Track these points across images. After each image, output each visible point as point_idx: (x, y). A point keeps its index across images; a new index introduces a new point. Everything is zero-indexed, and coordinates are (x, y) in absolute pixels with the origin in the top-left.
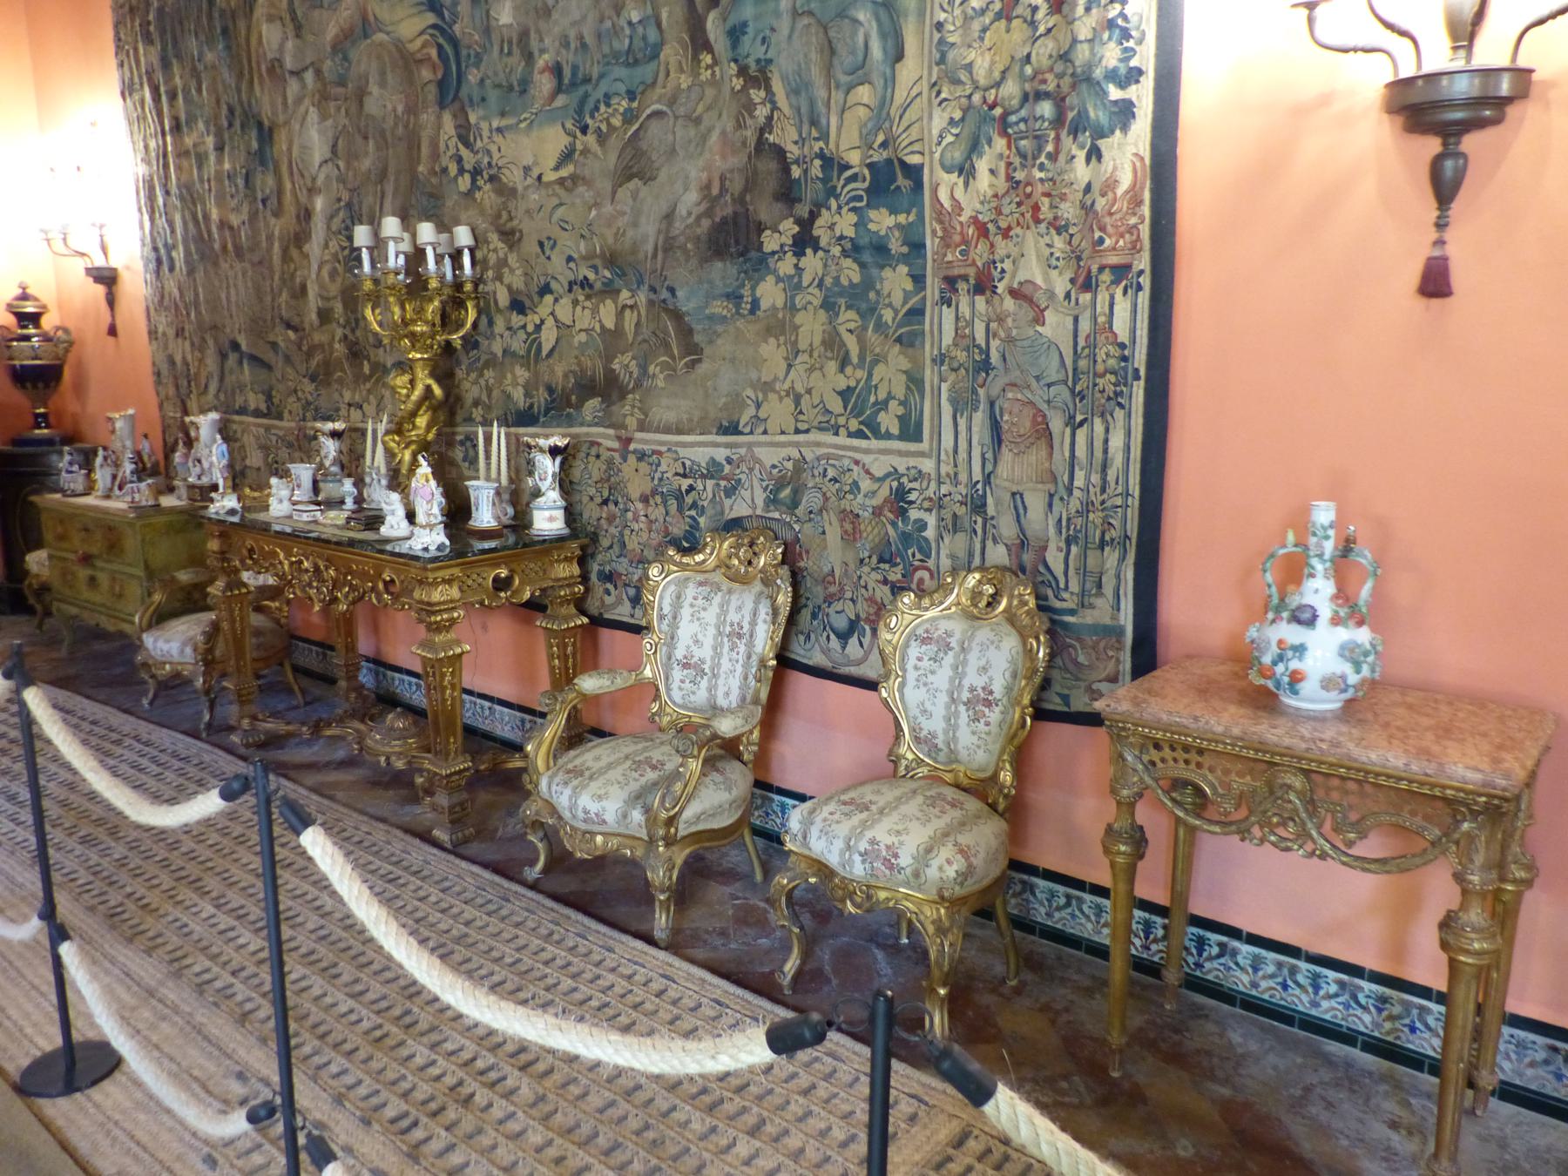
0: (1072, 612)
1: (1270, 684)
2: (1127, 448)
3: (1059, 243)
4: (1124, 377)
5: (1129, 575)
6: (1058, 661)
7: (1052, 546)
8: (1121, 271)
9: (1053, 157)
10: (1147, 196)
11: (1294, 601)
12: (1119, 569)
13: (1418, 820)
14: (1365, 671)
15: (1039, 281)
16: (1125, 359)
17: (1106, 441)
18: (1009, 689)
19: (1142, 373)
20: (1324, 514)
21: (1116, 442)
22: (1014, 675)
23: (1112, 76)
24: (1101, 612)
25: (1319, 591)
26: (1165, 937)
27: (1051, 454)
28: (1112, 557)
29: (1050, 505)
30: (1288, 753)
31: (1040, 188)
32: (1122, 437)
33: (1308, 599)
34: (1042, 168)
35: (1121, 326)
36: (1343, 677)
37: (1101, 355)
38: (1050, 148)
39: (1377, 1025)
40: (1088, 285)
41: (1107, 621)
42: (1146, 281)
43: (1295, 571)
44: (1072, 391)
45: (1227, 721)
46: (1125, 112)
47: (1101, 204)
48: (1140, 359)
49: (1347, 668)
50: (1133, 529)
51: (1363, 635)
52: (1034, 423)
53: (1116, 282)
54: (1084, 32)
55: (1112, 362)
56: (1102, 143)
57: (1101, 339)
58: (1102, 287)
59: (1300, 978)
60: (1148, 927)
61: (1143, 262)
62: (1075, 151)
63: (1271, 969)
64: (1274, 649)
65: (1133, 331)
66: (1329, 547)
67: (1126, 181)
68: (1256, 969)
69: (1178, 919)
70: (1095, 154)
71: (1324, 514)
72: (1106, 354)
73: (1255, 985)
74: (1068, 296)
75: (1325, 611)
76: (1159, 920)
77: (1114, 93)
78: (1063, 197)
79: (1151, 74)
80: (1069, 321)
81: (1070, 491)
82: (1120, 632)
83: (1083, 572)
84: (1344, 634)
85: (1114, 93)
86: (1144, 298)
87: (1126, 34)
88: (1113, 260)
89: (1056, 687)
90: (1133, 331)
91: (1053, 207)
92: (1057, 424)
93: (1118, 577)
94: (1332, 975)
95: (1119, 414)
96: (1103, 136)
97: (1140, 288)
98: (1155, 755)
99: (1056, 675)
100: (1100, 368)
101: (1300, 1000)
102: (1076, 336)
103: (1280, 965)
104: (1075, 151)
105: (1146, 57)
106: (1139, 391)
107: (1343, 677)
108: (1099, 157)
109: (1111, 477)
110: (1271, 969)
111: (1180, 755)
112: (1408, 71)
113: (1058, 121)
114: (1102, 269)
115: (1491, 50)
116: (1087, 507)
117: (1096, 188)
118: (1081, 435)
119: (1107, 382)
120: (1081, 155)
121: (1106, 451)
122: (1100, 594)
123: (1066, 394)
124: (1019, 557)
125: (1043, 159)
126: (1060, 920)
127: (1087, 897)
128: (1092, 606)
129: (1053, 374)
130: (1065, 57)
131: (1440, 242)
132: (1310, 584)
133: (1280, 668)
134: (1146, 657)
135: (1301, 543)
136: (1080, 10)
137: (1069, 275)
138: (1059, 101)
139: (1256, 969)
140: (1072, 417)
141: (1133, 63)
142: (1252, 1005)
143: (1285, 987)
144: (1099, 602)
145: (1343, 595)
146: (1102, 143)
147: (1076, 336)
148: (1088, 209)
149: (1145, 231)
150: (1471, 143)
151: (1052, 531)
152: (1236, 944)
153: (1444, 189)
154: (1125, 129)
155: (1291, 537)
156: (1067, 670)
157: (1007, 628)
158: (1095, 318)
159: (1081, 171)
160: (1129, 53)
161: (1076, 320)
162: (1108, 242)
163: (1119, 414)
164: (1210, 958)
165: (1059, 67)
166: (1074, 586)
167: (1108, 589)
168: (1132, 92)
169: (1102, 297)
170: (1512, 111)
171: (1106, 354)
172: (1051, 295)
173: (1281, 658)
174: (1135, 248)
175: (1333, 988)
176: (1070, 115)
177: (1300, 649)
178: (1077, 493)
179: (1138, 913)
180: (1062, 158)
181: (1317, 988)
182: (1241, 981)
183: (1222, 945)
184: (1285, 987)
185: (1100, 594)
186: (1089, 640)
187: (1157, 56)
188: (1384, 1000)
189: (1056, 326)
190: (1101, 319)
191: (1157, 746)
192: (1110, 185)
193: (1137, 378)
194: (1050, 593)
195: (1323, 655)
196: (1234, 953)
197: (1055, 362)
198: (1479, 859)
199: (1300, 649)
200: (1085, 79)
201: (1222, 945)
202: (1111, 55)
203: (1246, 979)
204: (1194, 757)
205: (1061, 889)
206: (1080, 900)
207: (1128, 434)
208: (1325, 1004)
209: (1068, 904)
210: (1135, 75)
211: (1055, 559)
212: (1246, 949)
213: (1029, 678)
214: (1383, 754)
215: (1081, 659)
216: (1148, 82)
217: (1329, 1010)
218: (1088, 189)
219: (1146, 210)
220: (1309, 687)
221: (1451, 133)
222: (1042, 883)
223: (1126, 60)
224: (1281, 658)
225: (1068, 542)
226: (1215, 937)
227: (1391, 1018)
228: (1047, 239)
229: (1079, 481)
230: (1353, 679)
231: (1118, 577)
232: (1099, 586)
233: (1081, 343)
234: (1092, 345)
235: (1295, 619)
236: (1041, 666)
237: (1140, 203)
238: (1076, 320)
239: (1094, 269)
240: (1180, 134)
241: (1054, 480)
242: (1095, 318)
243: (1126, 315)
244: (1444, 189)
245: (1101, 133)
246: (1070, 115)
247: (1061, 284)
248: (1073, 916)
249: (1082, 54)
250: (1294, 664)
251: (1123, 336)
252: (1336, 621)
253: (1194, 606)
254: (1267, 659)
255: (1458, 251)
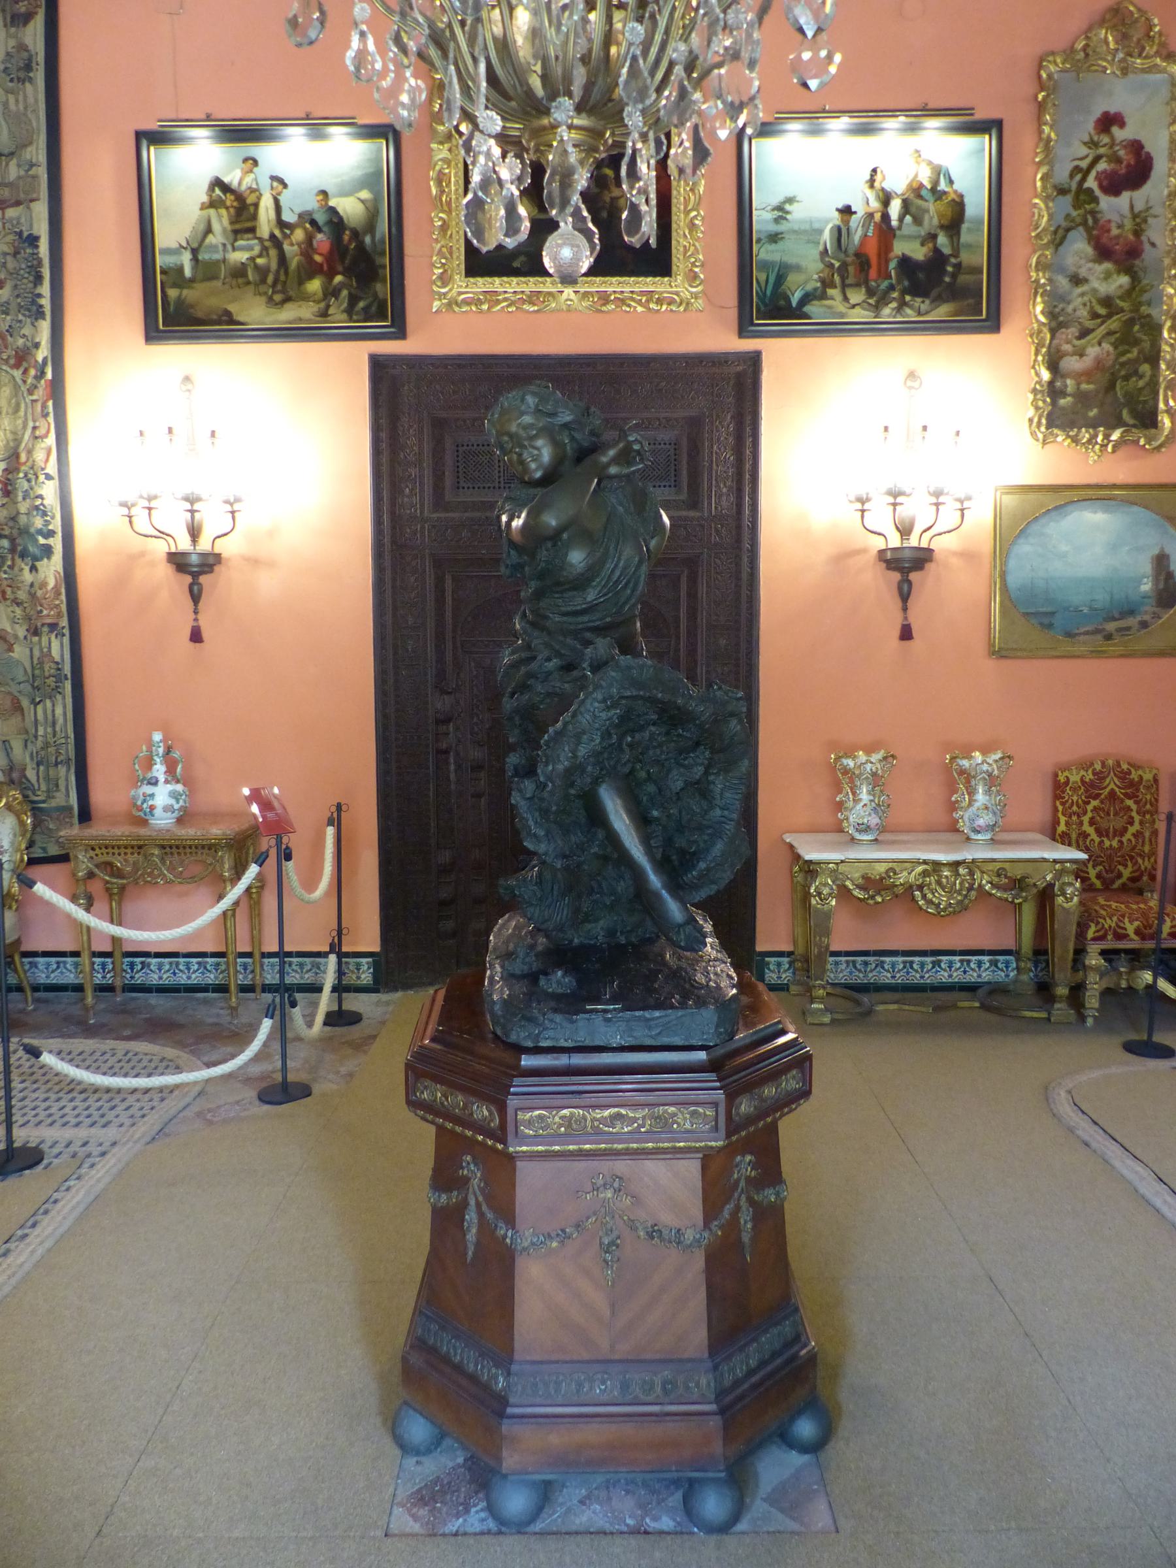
0: (44, 802)
1: (141, 814)
2: (65, 714)
3: (18, 611)
4: (59, 678)
5: (73, 778)
6: (38, 829)
7: (29, 768)
8: (53, 627)
9: (11, 567)
10: (63, 591)
11: (149, 775)
12: (67, 776)
13: (204, 856)
14: (181, 803)
15: (9, 630)
16: (59, 669)
17: (53, 711)
18: (12, 843)
19: (69, 676)
20: (157, 737)
21: (59, 711)
22: (15, 835)
23: (40, 532)
24: (59, 800)
25: (159, 770)
26: (113, 969)
27: (23, 719)
28: (62, 770)
29: (26, 746)
30: (150, 838)
31: (5, 583)
32: (62, 709)
33: (155, 774)
34: (5, 572)
35: (55, 652)
36: (172, 806)
37: (47, 668)
38: (9, 563)
39: (216, 978)
40: (36, 632)
41: (63, 803)
42: (66, 631)
43: (149, 763)
44: (33, 686)
45: (122, 831)
46: (48, 551)
47: (39, 593)
48: (67, 669)
49: (173, 802)
50: (72, 755)
51: (179, 787)
52: (13, 703)
53: (51, 632)
54: (23, 510)
55: (52, 671)
56: (37, 564)
57: (46, 659)
58: (44, 634)
59: (181, 967)
60: (104, 965)
61: (64, 622)
62: (23, 566)
63: (167, 967)
64: (142, 797)
65: (62, 656)
66: (161, 750)
67: (51, 583)
68: (160, 970)
69: (117, 955)
70: (34, 569)
71: (157, 737)
72: (49, 668)
73: (161, 978)
74: (25, 638)
75: (162, 778)
76: (109, 960)
77: (42, 541)
78: (19, 588)
79: (60, 534)
80: (27, 651)
81: (36, 737)
82: (70, 808)
83: (47, 779)
84: (170, 787)
85: (42, 541)
86: (66, 640)
87: (45, 514)
88: (49, 621)
89: (39, 844)
90: (62, 656)
91: (13, 592)
92: (25, 703)
93: (67, 780)
94: (194, 960)
95: (59, 697)
96: (38, 560)
97: (64, 635)
98: (92, 853)
99: (37, 837)
100: (47, 674)
101: (182, 979)
102: (32, 658)
103: (171, 963)
104: (23, 566)
105: (57, 524)
106: (68, 685)
107: (172, 806)
108: (37, 570)
109: (58, 729)
110: (167, 967)
111: (104, 850)
112: (173, 550)
113: (13, 550)
114: (43, 625)
115: (204, 545)
116: (46, 745)
117: (36, 585)
118: (40, 708)
119: (51, 681)
120: (27, 569)
121: (54, 716)
122: (58, 790)
123: (29, 688)
124: (10, 775)
125: (5, 568)
126: (55, 978)
127: (69, 960)
128: (53, 797)
129: (21, 677)
130: (14, 519)
131: (196, 620)
132: (156, 767)
133: (145, 806)
134: (85, 815)
135: (149, 750)
136: (20, 498)
137: (25, 627)
138: (13, 541)
139: (160, 970)
140: (34, 699)
141: (50, 527)
142: (162, 989)
143: (174, 974)
144: (57, 794)
145: (171, 771)
146: (37, 564)
147: (32, 658)
148: (33, 595)
149: (64, 607)
150: (203, 579)
151: (28, 759)
152: (149, 960)
153: (196, 596)
154: (49, 558)
155: (144, 748)
156: (43, 833)
157: (8, 813)
158: (41, 650)
159: (27, 576)
160: (47, 523)
161: (31, 650)
162: (45, 612)
163: (59, 697)
164: (138, 972)
165: (11, 524)
166: (43, 787)
167: (62, 787)
168: (51, 541)
169: (44, 639)
170: (216, 568)
171: (49, 668)
172: (16, 637)
173: (145, 801)
174: (59, 615)
175: (196, 967)
176: (19, 548)
177: (152, 796)
178: (40, 739)
179: (97, 960)
180: (16, 569)
181: (189, 969)
182: (154, 979)
183: (142, 963)
184: (174, 974)
185: (58, 790)
186: (55, 815)
187: (62, 526)
188: (218, 964)
189: (20, 652)
190: (45, 650)
191: (93, 849)
192: (43, 585)
193: (66, 679)
194: (30, 793)
195: (162, 797)
196: (149, 965)
197: (21, 672)
198: (227, 866)
199: (152, 796)
200: (25, 531)
201: (142, 963)
202: (38, 523)
203: (156, 976)
204: (110, 850)
205: (53, 960)
206: (65, 963)
207: (65, 707)
208: (193, 976)
209: (58, 967)
210: (51, 534)
211: (31, 774)
212: (154, 961)
213: (23, 835)
214: (189, 832)
215: (51, 826)
216: (59, 535)
217: (196, 978)
218: (32, 585)
219: (63, 597)
220: (158, 812)
221: (195, 575)
222: (41, 960)
223: (46, 525)
224: (145, 801)
225: (38, 764)
226: (138, 960)
227: (222, 972)
228: (11, 609)
229: (41, 732)
230: (176, 807)
231: (67, 780)
232: (57, 786)
233: (35, 661)
234: (41, 663)
235: (149, 783)
236: (30, 828)
237: (60, 594)
238: (31, 650)
239: (39, 624)
240: (78, 571)
241: (27, 732)
242: (41, 650)
243: (58, 648)
244: (196, 596)
245: (36, 559)
246: (19, 548)
247: (21, 632)
248: (62, 973)
249: (23, 520)
250: (151, 803)
251: (57, 658)
252: (167, 782)
253: (105, 793)
254: (139, 803)
255: (203, 623)
